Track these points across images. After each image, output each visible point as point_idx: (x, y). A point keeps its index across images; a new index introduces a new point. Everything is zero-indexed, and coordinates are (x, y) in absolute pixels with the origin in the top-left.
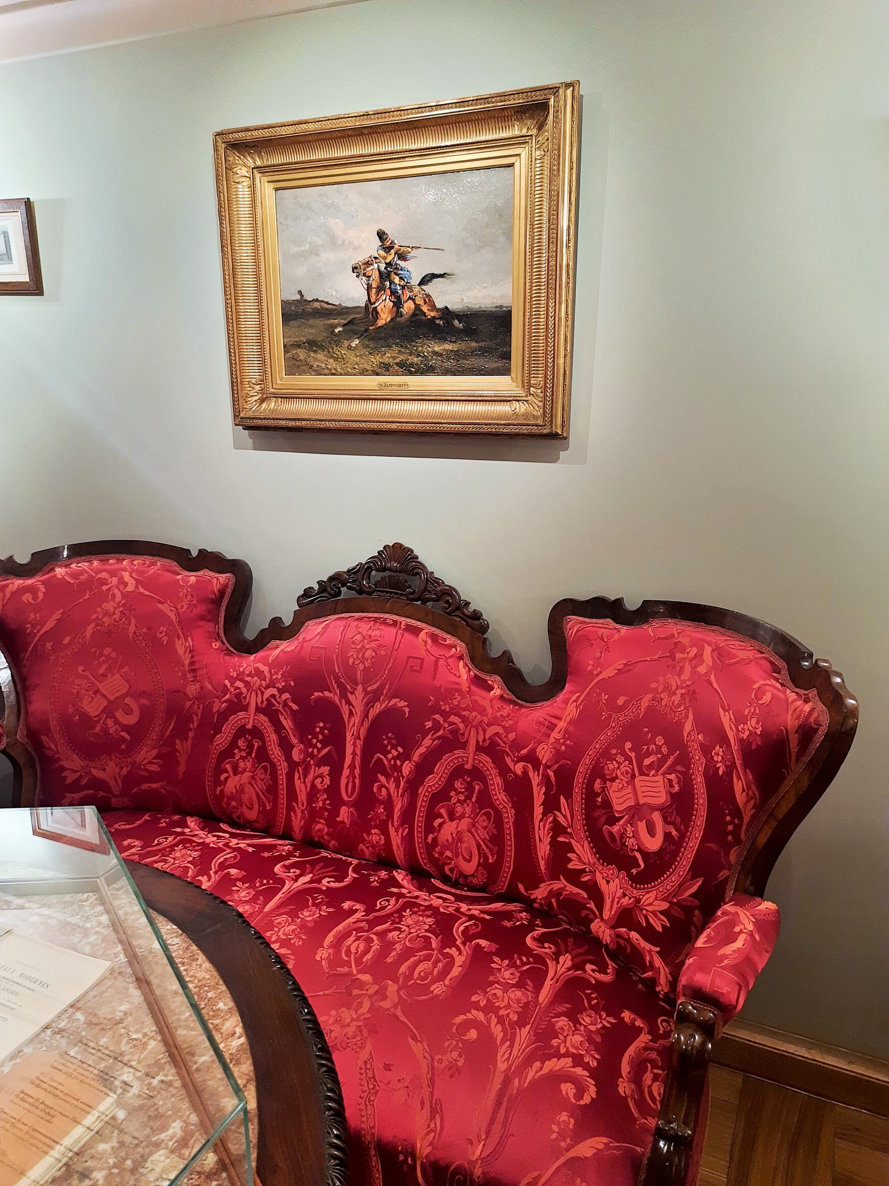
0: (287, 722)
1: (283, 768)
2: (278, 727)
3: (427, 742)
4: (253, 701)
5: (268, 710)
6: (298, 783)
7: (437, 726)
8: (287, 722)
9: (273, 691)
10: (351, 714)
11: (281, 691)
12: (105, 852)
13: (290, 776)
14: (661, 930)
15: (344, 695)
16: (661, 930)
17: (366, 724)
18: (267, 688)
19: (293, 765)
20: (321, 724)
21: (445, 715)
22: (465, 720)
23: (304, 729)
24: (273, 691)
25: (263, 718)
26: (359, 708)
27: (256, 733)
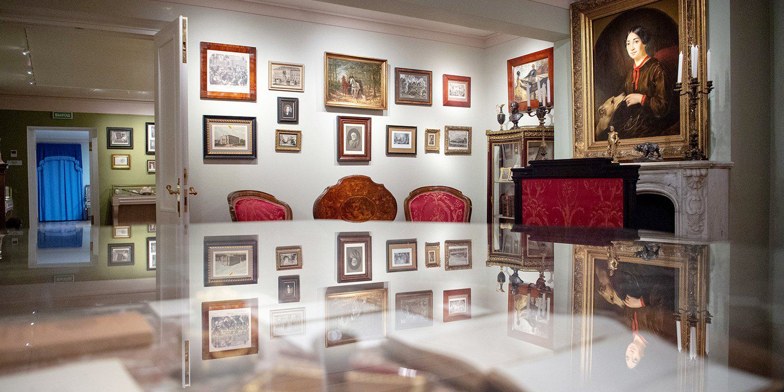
0: (546, 219)
1: (449, 212)
2: (543, 221)
3: (592, 222)
4: (534, 213)
5: (539, 215)
6: (453, 215)
7: (594, 215)
8: (546, 219)
9: (539, 208)
10: (566, 215)
11: (542, 208)
12: (523, 115)
13: (451, 214)
14: (632, 37)
15: (562, 208)
16: (632, 37)
17: (571, 218)
18: (612, 211)
19: (452, 211)
20: (556, 219)
21: (597, 211)
22: (603, 211)
23: (551, 221)
24: (539, 208)
25: (538, 219)
26: (568, 212)
27: (536, 224)
